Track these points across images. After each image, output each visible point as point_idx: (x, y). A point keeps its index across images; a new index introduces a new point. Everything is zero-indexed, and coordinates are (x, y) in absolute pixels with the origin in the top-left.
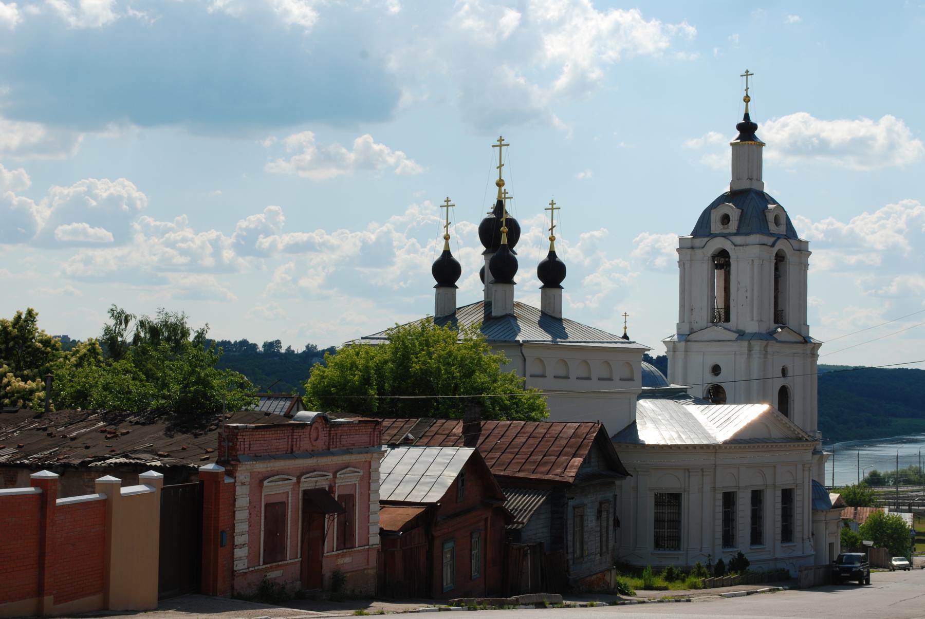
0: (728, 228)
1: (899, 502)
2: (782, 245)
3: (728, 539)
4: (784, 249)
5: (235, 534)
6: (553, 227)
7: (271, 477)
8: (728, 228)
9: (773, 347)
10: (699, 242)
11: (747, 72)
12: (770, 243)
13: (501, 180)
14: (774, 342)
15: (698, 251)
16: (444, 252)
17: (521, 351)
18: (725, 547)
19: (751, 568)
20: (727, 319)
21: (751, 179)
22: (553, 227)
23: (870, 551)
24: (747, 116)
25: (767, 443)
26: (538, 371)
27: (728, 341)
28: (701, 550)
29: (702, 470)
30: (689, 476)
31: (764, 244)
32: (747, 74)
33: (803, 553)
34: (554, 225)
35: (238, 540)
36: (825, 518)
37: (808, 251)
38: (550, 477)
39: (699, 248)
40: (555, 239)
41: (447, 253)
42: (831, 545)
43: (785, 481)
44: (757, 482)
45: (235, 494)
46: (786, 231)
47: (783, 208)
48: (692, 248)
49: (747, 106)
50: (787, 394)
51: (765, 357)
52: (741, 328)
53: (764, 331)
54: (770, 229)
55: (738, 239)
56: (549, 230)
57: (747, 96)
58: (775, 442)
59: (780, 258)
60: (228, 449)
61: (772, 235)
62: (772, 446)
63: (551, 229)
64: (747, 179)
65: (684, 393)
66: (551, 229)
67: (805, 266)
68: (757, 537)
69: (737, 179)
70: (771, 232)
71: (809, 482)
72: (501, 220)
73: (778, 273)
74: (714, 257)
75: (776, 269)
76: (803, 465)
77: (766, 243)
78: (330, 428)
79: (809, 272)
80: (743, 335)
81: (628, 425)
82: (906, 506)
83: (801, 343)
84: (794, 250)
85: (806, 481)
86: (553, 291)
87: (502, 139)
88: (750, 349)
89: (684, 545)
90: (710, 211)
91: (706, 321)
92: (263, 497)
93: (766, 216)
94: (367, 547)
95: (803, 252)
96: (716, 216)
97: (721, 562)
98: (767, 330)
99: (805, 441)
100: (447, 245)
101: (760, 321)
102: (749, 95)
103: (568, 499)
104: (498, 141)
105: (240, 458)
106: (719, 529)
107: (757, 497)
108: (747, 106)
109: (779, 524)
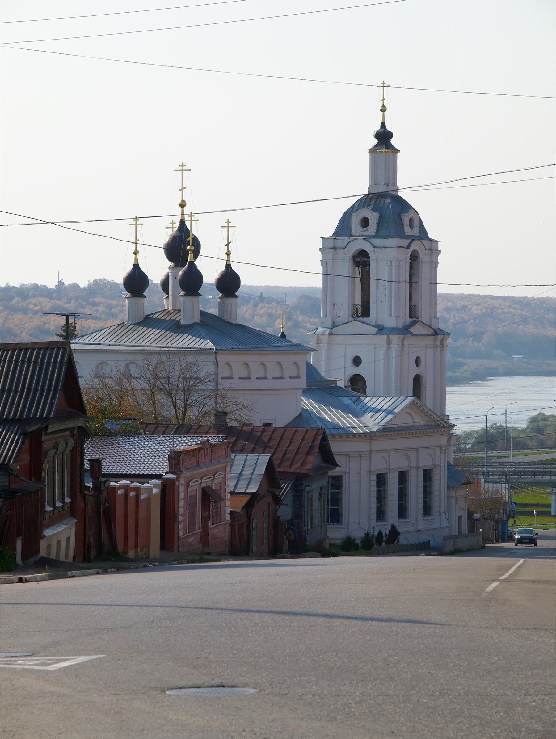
0: (367, 230)
1: (489, 471)
2: (416, 246)
3: (381, 515)
4: (420, 252)
5: (179, 515)
6: (229, 243)
7: (192, 480)
8: (367, 230)
9: (409, 341)
10: (343, 240)
11: (384, 83)
12: (406, 245)
13: (183, 201)
14: (410, 335)
15: (340, 252)
16: (134, 265)
17: (216, 357)
18: (378, 521)
19: (402, 540)
20: (366, 312)
21: (388, 185)
22: (229, 243)
23: (477, 523)
24: (383, 125)
25: (412, 430)
26: (227, 374)
27: (368, 335)
28: (359, 524)
29: (360, 456)
30: (349, 461)
31: (401, 247)
32: (384, 86)
33: (440, 525)
34: (229, 242)
35: (181, 518)
36: (456, 494)
37: (438, 250)
38: (292, 470)
39: (341, 248)
40: (231, 254)
41: (136, 267)
42: (460, 517)
43: (426, 462)
44: (403, 464)
45: (179, 491)
46: (419, 232)
47: (416, 211)
48: (334, 248)
49: (383, 115)
50: (420, 382)
51: (402, 350)
52: (380, 322)
53: (400, 326)
54: (405, 232)
55: (378, 242)
56: (226, 245)
57: (383, 106)
58: (419, 429)
59: (414, 257)
60: (175, 465)
61: (407, 237)
62: (416, 433)
63: (227, 245)
64: (384, 184)
65: (334, 385)
66: (227, 245)
67: (435, 264)
68: (403, 512)
69: (375, 184)
70: (407, 234)
71: (445, 463)
72: (188, 239)
73: (411, 271)
74: (354, 257)
75: (411, 268)
76: (441, 449)
77: (402, 245)
78: (212, 448)
79: (439, 269)
80: (382, 329)
81: (295, 417)
82: (496, 475)
83: (432, 335)
84: (426, 250)
85: (443, 461)
86: (230, 300)
87: (184, 164)
88: (389, 343)
89: (345, 519)
90: (351, 214)
91: (347, 315)
92: (188, 492)
93: (401, 219)
94: (225, 522)
95: (434, 251)
96: (355, 220)
97: (380, 533)
98: (403, 325)
99: (442, 427)
100: (136, 259)
101: (398, 317)
102: (385, 105)
103: (306, 486)
104: (180, 166)
105: (182, 469)
106: (374, 506)
107: (403, 477)
108: (383, 115)
109: (421, 500)
